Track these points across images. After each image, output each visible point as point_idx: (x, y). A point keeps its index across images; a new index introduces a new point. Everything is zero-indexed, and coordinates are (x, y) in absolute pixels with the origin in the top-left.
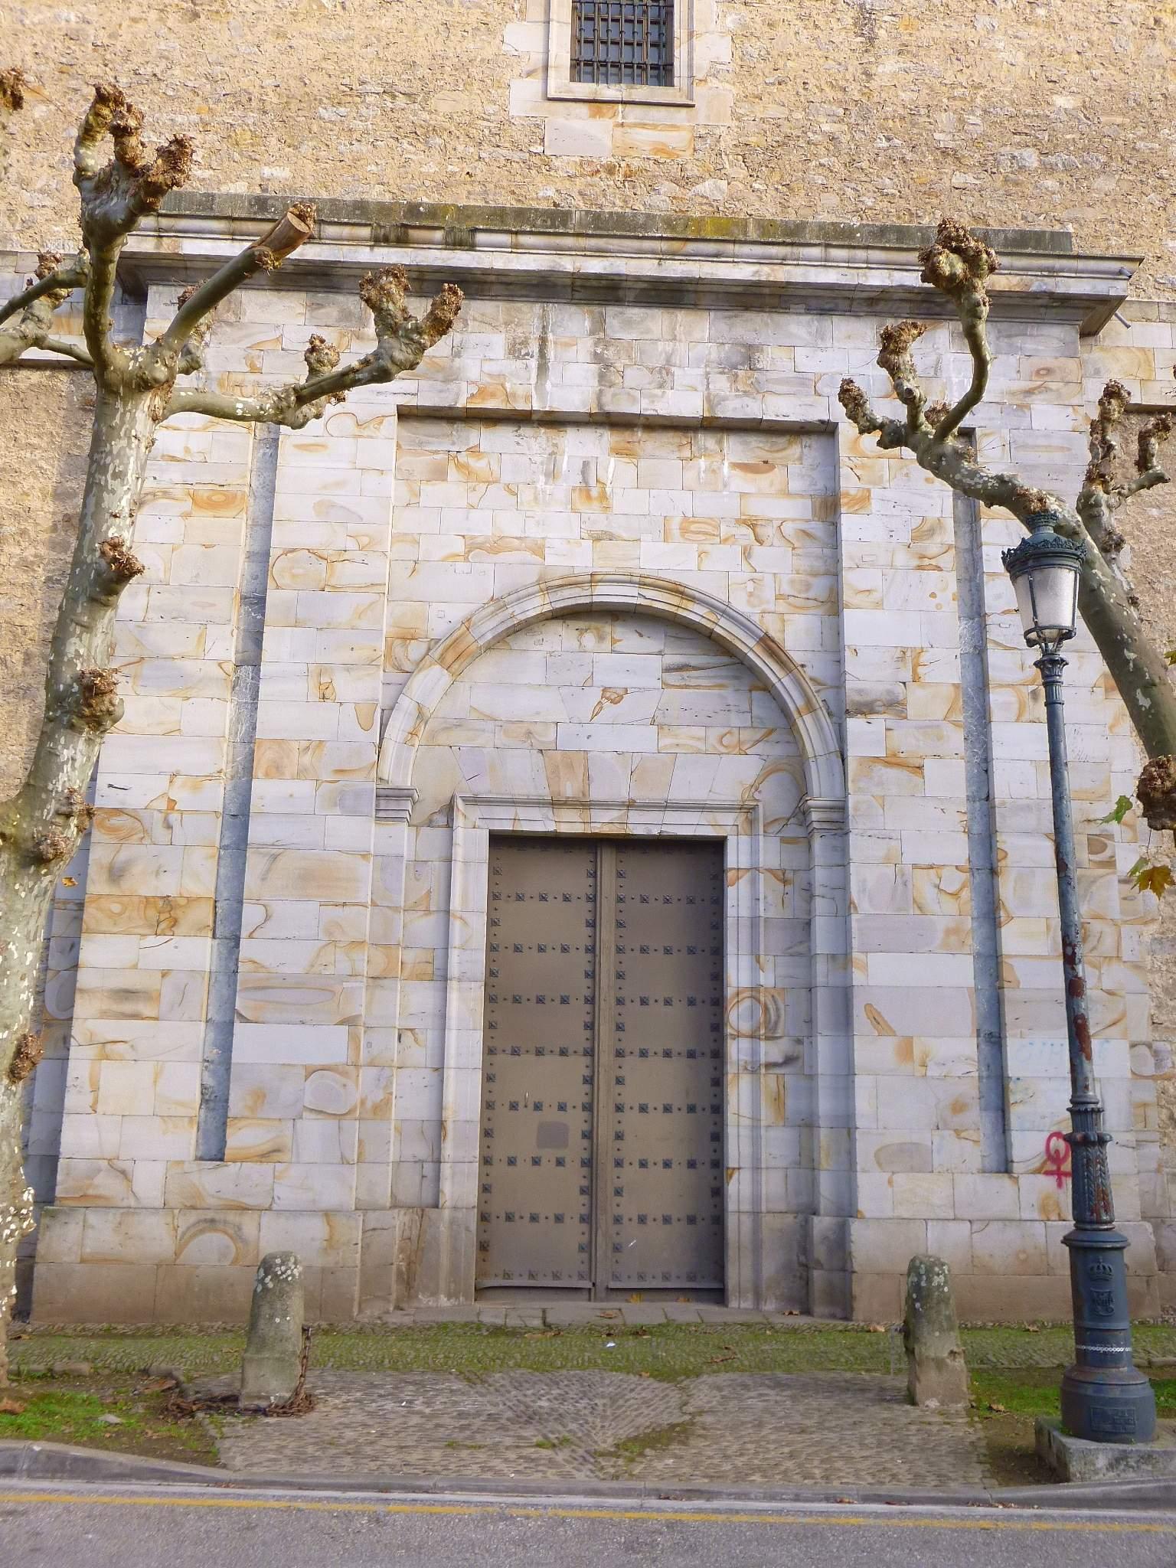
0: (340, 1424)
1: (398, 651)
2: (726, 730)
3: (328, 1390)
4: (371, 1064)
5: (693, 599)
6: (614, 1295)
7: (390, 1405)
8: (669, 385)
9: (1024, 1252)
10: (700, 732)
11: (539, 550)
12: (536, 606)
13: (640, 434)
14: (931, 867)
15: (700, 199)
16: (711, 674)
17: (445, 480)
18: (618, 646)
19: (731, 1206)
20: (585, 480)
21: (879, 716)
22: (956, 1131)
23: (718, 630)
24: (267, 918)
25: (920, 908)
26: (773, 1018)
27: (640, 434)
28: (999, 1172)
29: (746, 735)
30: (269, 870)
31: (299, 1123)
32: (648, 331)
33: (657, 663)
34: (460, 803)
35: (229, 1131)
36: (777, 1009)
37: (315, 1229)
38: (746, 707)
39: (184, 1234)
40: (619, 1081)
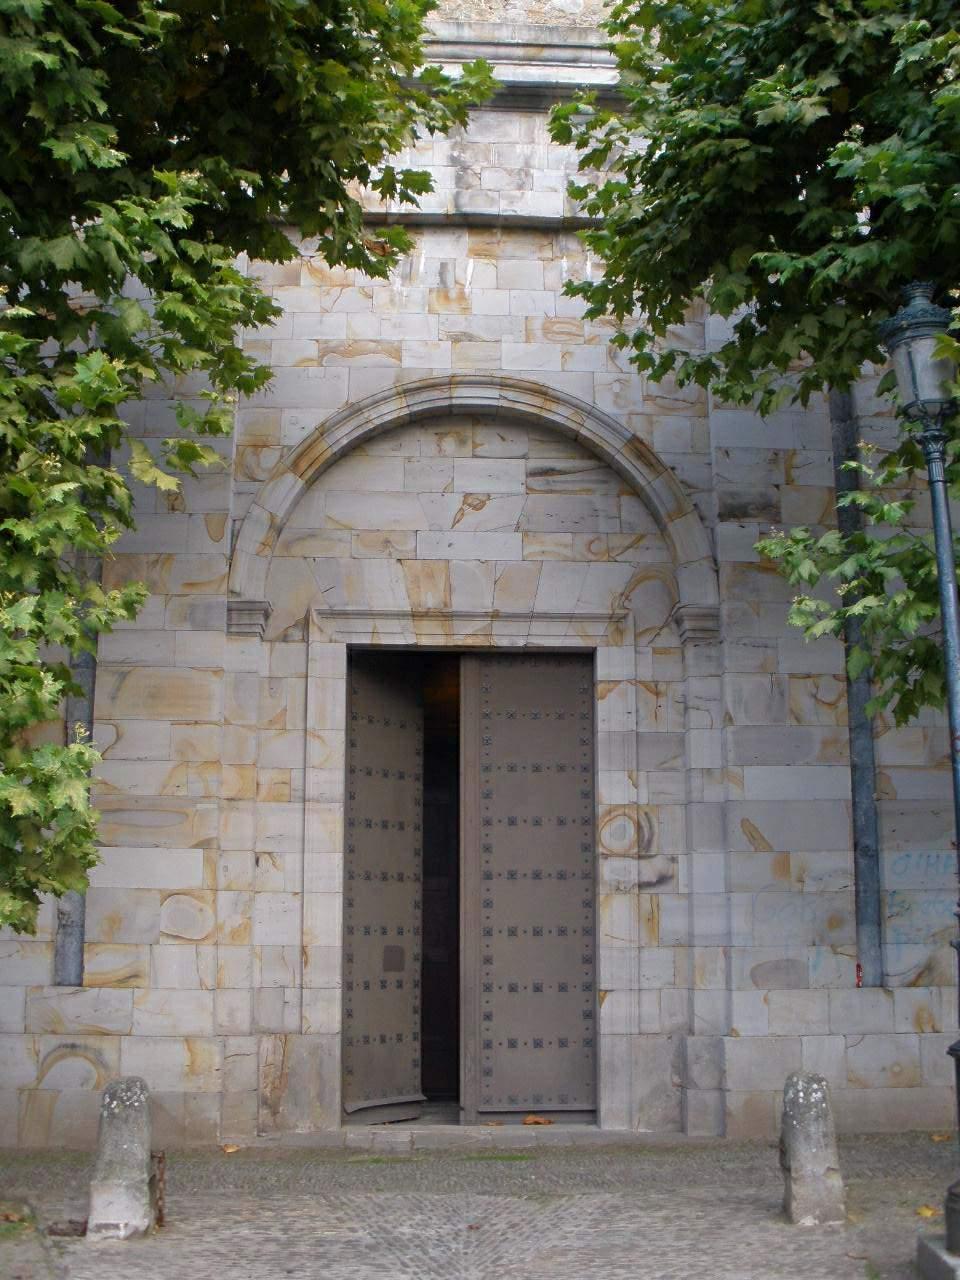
0: (191, 1252)
1: (250, 459)
2: (595, 536)
3: (182, 1216)
4: (228, 889)
5: (557, 400)
6: (484, 1118)
7: (245, 1231)
8: (527, 186)
9: (899, 1065)
10: (568, 538)
11: (396, 352)
12: (392, 410)
13: (499, 236)
14: (808, 676)
15: (556, 13)
16: (579, 478)
17: (298, 284)
18: (479, 451)
19: (605, 1028)
20: (443, 281)
21: (751, 520)
22: (832, 946)
23: (583, 431)
24: (119, 737)
25: (798, 719)
26: (646, 837)
27: (499, 235)
28: (874, 986)
29: (617, 541)
30: (118, 689)
31: (156, 948)
32: (506, 135)
33: (519, 467)
34: (314, 616)
35: (86, 956)
36: (651, 827)
37: (179, 1055)
38: (615, 512)
39: (45, 1059)
40: (488, 904)
